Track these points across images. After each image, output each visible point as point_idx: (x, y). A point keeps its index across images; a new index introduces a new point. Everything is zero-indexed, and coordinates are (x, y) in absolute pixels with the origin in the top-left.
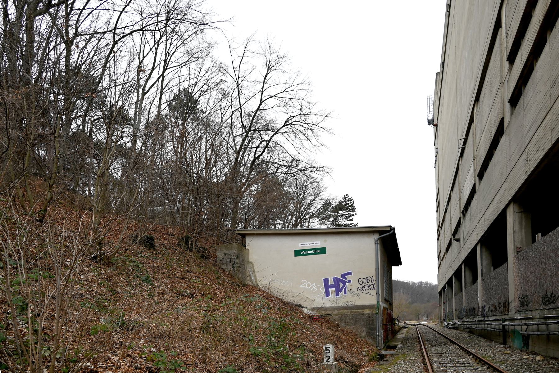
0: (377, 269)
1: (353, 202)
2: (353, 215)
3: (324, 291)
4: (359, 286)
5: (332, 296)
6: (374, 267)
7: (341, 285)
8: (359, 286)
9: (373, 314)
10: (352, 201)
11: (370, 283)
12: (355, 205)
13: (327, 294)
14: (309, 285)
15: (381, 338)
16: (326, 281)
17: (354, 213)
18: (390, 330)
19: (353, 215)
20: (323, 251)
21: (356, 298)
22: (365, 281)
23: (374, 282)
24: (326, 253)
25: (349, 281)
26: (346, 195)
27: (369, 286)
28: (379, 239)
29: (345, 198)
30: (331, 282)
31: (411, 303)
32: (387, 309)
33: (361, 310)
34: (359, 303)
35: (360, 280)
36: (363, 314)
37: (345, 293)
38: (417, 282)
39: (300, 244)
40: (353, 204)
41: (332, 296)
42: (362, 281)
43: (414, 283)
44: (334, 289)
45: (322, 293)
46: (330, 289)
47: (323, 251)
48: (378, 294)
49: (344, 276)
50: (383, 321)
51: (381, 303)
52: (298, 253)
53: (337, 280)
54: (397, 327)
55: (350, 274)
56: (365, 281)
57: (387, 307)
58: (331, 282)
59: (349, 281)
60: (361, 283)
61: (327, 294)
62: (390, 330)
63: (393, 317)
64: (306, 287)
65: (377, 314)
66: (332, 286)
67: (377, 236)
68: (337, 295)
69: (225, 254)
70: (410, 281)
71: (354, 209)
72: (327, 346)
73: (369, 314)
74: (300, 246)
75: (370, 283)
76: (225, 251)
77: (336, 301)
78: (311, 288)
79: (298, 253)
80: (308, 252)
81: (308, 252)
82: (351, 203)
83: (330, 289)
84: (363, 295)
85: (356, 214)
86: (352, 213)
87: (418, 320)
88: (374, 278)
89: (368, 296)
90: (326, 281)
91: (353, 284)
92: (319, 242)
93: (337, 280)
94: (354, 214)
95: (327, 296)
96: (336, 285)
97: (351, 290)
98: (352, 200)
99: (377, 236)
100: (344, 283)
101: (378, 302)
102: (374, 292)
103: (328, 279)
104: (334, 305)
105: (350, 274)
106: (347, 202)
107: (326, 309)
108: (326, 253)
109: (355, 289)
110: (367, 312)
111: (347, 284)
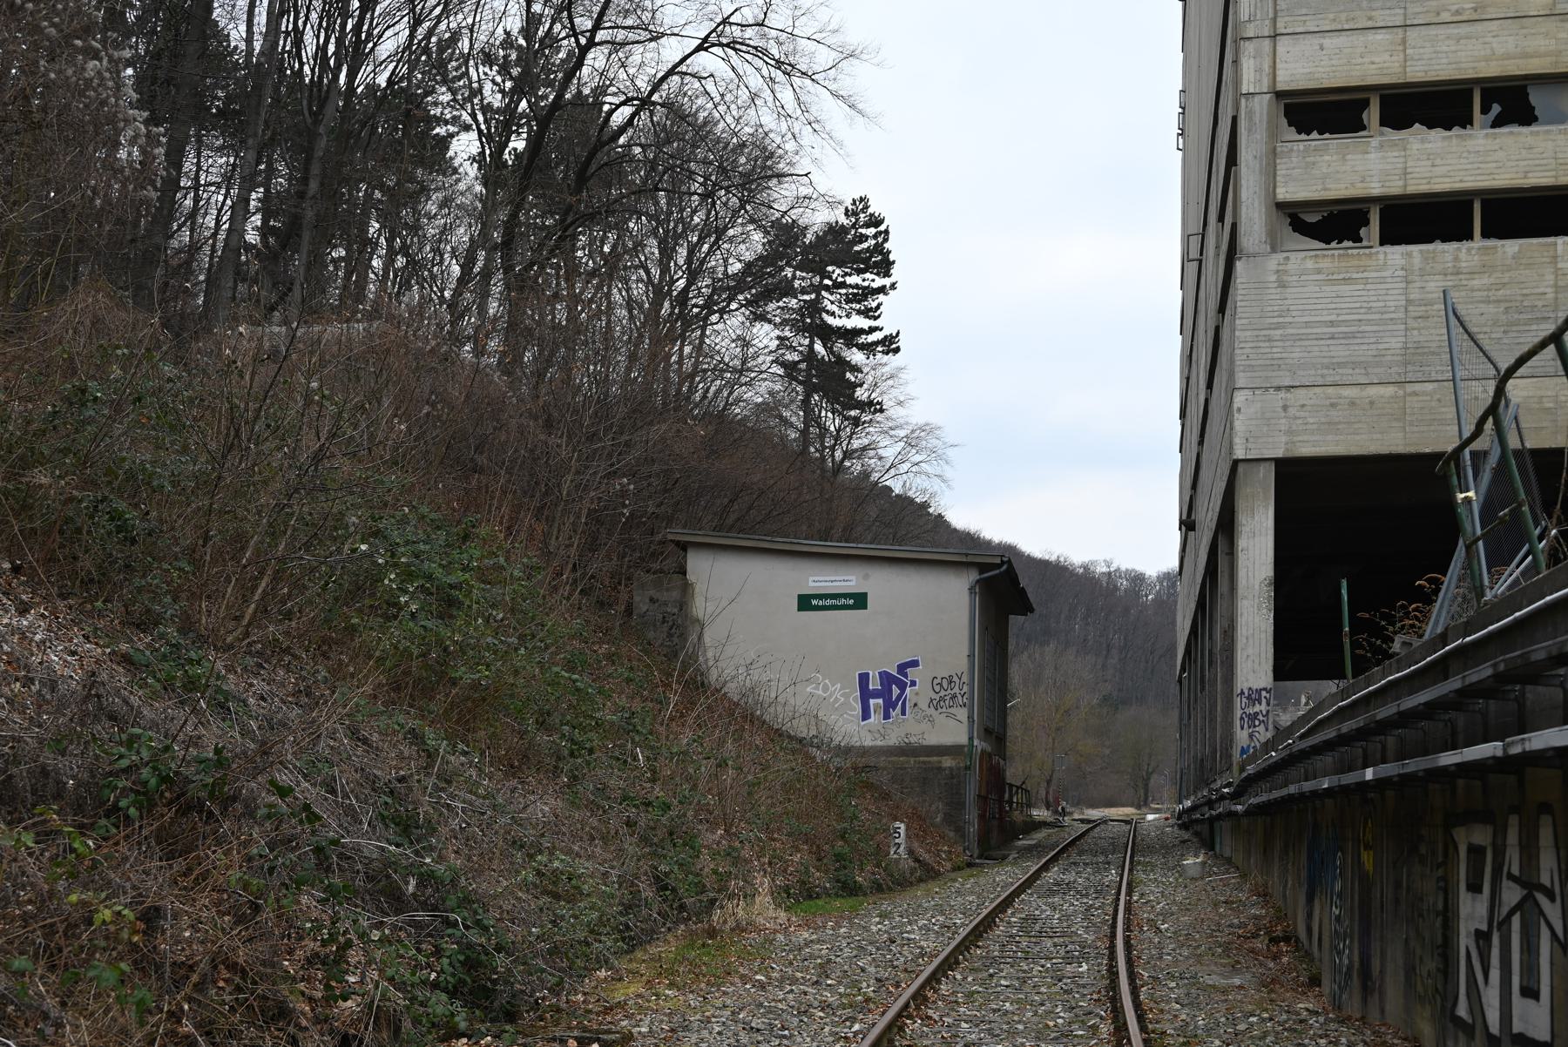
0: (971, 656)
1: (887, 232)
2: (882, 290)
3: (858, 707)
4: (934, 696)
5: (875, 719)
6: (966, 652)
7: (896, 691)
8: (934, 696)
9: (959, 769)
10: (882, 228)
11: (956, 690)
12: (895, 247)
13: (866, 715)
14: (825, 689)
15: (973, 829)
16: (864, 678)
17: (887, 282)
18: (994, 818)
19: (882, 290)
20: (860, 601)
21: (925, 726)
22: (945, 684)
23: (965, 689)
24: (866, 608)
25: (913, 683)
26: (862, 199)
27: (954, 697)
28: (978, 581)
29: (855, 214)
30: (875, 684)
31: (1112, 703)
32: (990, 755)
33: (935, 759)
34: (933, 739)
35: (936, 681)
36: (940, 769)
37: (903, 713)
38: (1154, 574)
39: (811, 579)
40: (886, 240)
41: (875, 719)
42: (940, 684)
43: (1138, 579)
44: (880, 701)
45: (854, 710)
46: (872, 701)
47: (860, 601)
48: (971, 717)
49: (902, 668)
50: (980, 787)
51: (976, 742)
52: (805, 603)
53: (886, 678)
54: (1017, 816)
55: (914, 664)
56: (945, 684)
57: (989, 749)
58: (875, 684)
59: (913, 683)
60: (937, 688)
61: (866, 715)
62: (994, 818)
63: (1004, 779)
64: (820, 692)
65: (967, 768)
66: (876, 694)
67: (974, 576)
68: (887, 716)
69: (652, 600)
70: (1123, 568)
71: (885, 267)
72: (897, 824)
73: (951, 769)
74: (812, 584)
75: (956, 690)
76: (652, 592)
77: (882, 731)
78: (831, 696)
79: (805, 603)
80: (829, 602)
81: (829, 602)
82: (875, 236)
83: (872, 701)
84: (940, 719)
85: (893, 286)
86: (879, 282)
87: (1146, 804)
88: (965, 679)
89: (952, 722)
90: (864, 678)
91: (919, 691)
92: (853, 578)
93: (886, 678)
94: (884, 287)
95: (864, 719)
96: (884, 693)
97: (915, 705)
98: (882, 221)
99: (974, 576)
100: (902, 687)
101: (971, 739)
102: (962, 714)
103: (867, 675)
104: (879, 743)
105: (914, 664)
106: (863, 231)
107: (864, 751)
108: (866, 608)
109: (923, 704)
110: (947, 762)
111: (908, 689)
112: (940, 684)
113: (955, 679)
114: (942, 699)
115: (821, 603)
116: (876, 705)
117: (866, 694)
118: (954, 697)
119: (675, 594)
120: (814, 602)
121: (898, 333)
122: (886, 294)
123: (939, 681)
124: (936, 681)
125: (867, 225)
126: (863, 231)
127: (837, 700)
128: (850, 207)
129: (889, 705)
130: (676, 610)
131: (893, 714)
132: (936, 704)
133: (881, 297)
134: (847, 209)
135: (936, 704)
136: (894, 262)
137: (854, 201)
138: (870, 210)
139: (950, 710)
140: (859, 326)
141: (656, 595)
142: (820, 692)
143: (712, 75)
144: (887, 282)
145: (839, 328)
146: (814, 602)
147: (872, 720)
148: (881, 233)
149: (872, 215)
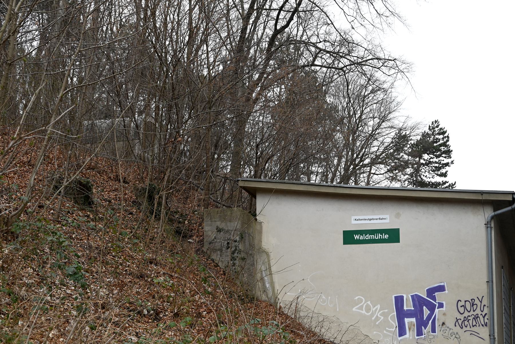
0: (490, 282)
1: (448, 137)
2: (447, 164)
3: (395, 323)
4: (459, 316)
7: (426, 312)
8: (459, 316)
10: (446, 135)
11: (478, 311)
13: (402, 332)
14: (368, 309)
16: (399, 301)
17: (449, 161)
19: (447, 164)
23: (486, 311)
25: (441, 305)
26: (436, 122)
27: (476, 317)
28: (492, 218)
30: (408, 305)
35: (460, 304)
37: (434, 331)
39: (353, 218)
40: (448, 141)
42: (464, 306)
44: (414, 320)
46: (407, 320)
48: (491, 335)
49: (431, 292)
53: (418, 300)
55: (441, 289)
58: (408, 305)
59: (441, 305)
60: (462, 310)
61: (402, 332)
64: (364, 312)
66: (410, 314)
67: (489, 213)
68: (419, 333)
69: (219, 230)
71: (448, 153)
75: (478, 311)
76: (218, 223)
78: (372, 315)
80: (368, 237)
81: (368, 237)
82: (443, 138)
83: (407, 320)
86: (446, 161)
88: (485, 302)
89: (475, 339)
90: (399, 301)
92: (387, 216)
93: (418, 300)
94: (448, 163)
95: (400, 335)
96: (417, 313)
97: (443, 324)
98: (446, 132)
99: (489, 213)
100: (432, 308)
102: (484, 332)
105: (441, 289)
106: (437, 136)
109: (450, 323)
111: (437, 310)
112: (464, 306)
113: (477, 302)
114: (466, 319)
115: (361, 238)
116: (411, 323)
117: (401, 314)
118: (476, 317)
119: (235, 225)
120: (356, 237)
121: (455, 182)
122: (449, 166)
123: (462, 303)
124: (460, 304)
125: (439, 134)
126: (437, 136)
127: (377, 318)
128: (431, 125)
129: (421, 324)
130: (238, 238)
131: (425, 331)
132: (461, 323)
133: (447, 168)
134: (430, 127)
135: (461, 323)
136: (452, 151)
137: (433, 122)
138: (440, 127)
139: (473, 329)
140: (438, 181)
141: (222, 225)
142: (364, 312)
143: (466, 301)
144: (449, 161)
145: (429, 182)
146: (356, 237)
147: (407, 336)
148: (445, 137)
149: (441, 129)
